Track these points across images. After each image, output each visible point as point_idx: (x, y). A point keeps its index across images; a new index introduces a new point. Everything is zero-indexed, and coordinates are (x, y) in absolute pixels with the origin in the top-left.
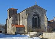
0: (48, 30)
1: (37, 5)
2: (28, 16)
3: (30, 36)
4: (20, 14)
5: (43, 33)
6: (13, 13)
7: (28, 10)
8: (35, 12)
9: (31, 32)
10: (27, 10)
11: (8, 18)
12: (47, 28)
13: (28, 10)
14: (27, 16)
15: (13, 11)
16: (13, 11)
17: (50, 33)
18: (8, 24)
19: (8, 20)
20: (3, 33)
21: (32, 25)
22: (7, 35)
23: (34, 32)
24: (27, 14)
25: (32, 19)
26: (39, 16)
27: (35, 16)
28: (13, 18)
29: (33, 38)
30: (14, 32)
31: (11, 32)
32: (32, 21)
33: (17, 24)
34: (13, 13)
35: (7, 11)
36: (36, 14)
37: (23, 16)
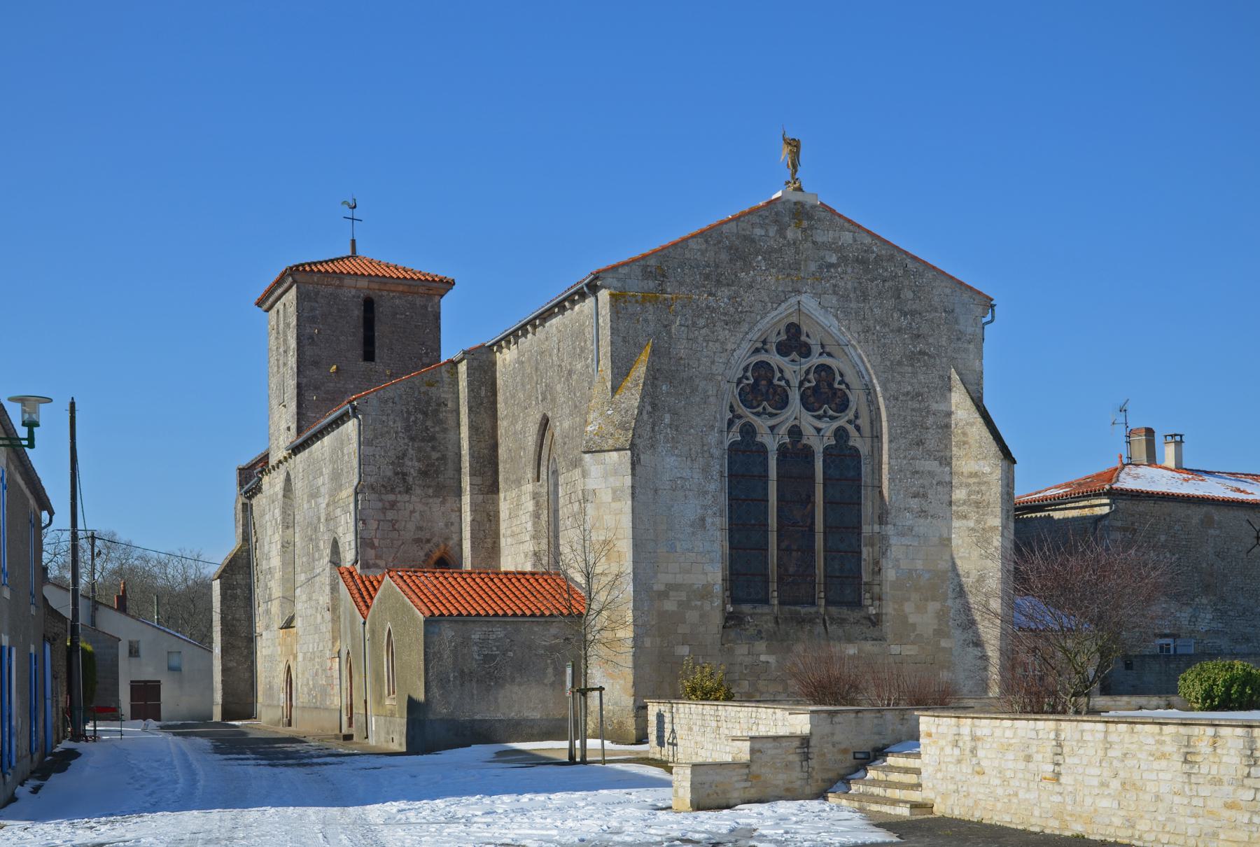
0: (1010, 660)
1: (817, 191)
2: (651, 401)
3: (682, 779)
4: (506, 358)
5: (927, 723)
6: (369, 356)
7: (646, 299)
8: (772, 321)
9: (708, 709)
10: (637, 286)
11: (282, 423)
12: (991, 633)
13: (646, 299)
14: (631, 397)
15: (369, 305)
16: (369, 305)
17: (1046, 726)
18: (270, 556)
19: (272, 484)
20: (183, 728)
21: (714, 575)
22: (254, 771)
23: (752, 697)
24: (621, 371)
25: (719, 466)
26: (843, 406)
27: (783, 403)
28: (300, 298)
29: (749, 815)
30: (394, 704)
31: (337, 700)
32: (717, 488)
33: (446, 562)
34: (369, 356)
35: (266, 301)
36: (792, 370)
37: (548, 395)
